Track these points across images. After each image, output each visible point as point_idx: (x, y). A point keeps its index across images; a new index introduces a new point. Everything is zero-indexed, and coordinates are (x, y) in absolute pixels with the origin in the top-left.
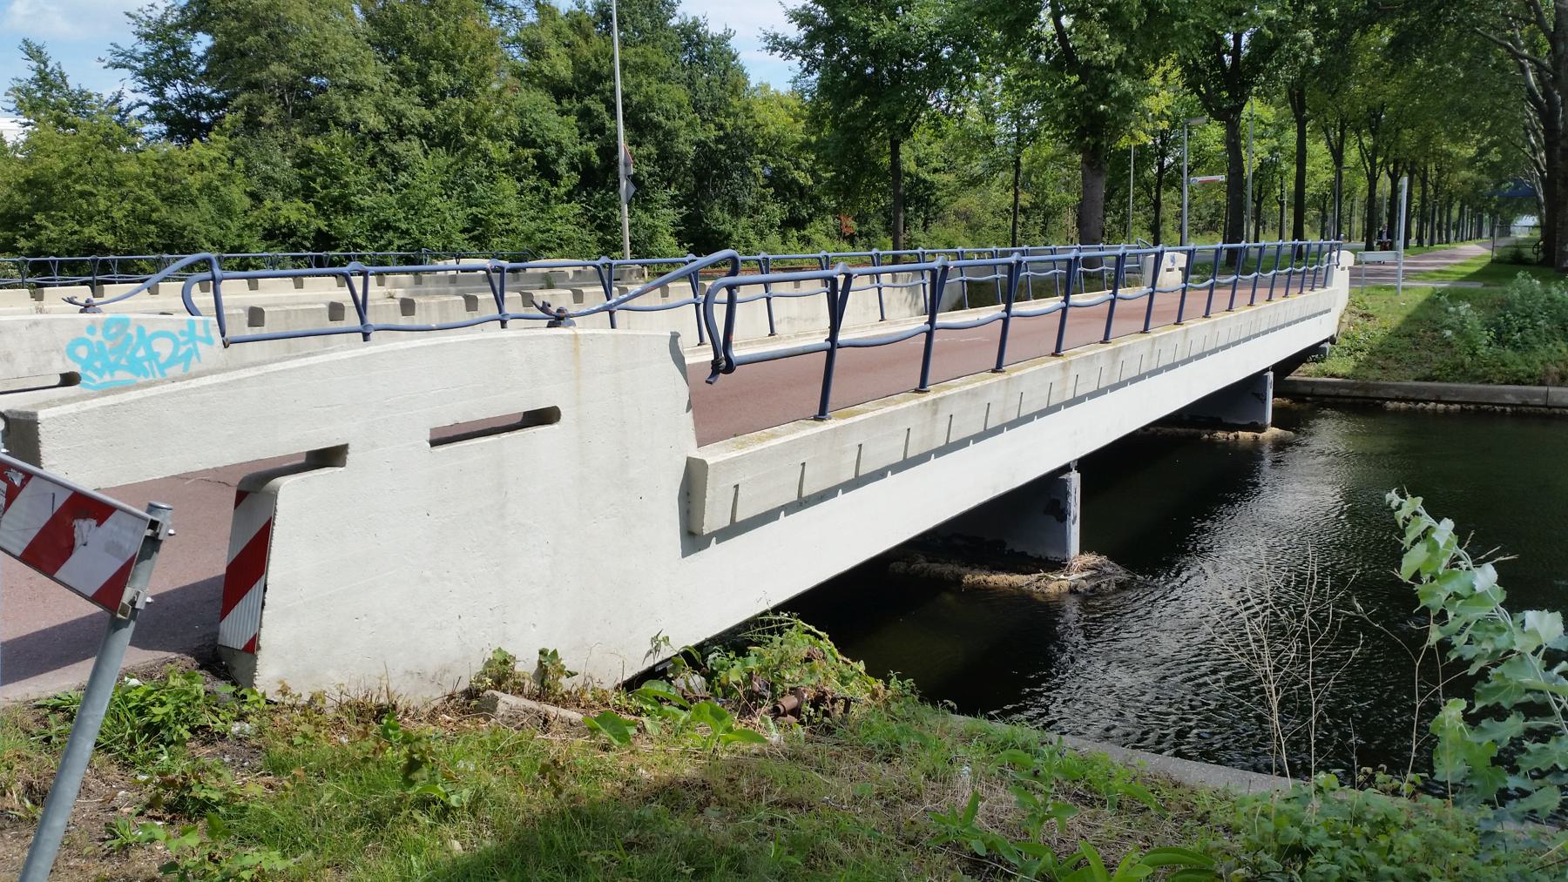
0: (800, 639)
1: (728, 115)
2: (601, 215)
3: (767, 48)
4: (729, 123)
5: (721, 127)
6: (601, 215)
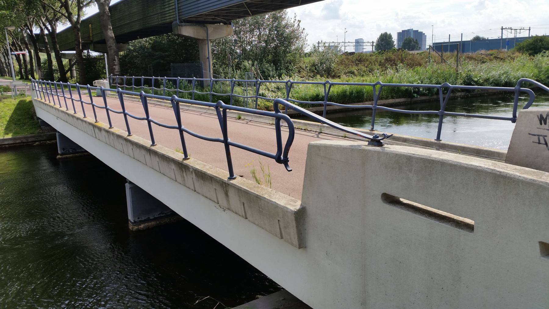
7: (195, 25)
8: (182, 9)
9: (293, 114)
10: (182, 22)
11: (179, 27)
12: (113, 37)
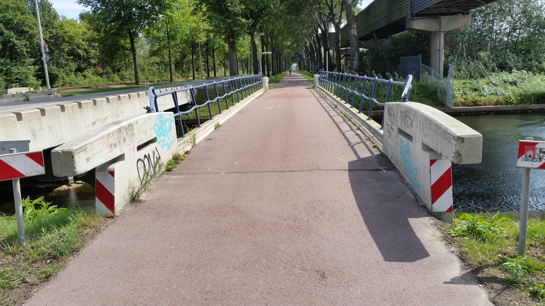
0: (523, 169)
1: (53, 28)
2: (5, 69)
3: (77, 2)
4: (54, 31)
5: (50, 32)
6: (5, 69)
7: (428, 18)
8: (414, 4)
9: (506, 111)
10: (414, 16)
11: (410, 21)
12: (356, 35)
